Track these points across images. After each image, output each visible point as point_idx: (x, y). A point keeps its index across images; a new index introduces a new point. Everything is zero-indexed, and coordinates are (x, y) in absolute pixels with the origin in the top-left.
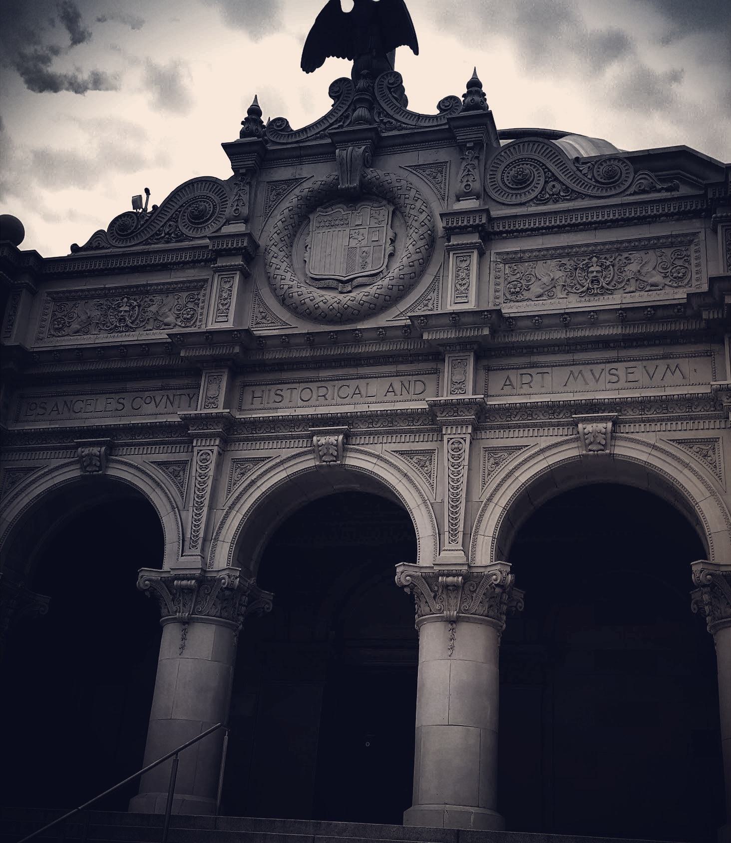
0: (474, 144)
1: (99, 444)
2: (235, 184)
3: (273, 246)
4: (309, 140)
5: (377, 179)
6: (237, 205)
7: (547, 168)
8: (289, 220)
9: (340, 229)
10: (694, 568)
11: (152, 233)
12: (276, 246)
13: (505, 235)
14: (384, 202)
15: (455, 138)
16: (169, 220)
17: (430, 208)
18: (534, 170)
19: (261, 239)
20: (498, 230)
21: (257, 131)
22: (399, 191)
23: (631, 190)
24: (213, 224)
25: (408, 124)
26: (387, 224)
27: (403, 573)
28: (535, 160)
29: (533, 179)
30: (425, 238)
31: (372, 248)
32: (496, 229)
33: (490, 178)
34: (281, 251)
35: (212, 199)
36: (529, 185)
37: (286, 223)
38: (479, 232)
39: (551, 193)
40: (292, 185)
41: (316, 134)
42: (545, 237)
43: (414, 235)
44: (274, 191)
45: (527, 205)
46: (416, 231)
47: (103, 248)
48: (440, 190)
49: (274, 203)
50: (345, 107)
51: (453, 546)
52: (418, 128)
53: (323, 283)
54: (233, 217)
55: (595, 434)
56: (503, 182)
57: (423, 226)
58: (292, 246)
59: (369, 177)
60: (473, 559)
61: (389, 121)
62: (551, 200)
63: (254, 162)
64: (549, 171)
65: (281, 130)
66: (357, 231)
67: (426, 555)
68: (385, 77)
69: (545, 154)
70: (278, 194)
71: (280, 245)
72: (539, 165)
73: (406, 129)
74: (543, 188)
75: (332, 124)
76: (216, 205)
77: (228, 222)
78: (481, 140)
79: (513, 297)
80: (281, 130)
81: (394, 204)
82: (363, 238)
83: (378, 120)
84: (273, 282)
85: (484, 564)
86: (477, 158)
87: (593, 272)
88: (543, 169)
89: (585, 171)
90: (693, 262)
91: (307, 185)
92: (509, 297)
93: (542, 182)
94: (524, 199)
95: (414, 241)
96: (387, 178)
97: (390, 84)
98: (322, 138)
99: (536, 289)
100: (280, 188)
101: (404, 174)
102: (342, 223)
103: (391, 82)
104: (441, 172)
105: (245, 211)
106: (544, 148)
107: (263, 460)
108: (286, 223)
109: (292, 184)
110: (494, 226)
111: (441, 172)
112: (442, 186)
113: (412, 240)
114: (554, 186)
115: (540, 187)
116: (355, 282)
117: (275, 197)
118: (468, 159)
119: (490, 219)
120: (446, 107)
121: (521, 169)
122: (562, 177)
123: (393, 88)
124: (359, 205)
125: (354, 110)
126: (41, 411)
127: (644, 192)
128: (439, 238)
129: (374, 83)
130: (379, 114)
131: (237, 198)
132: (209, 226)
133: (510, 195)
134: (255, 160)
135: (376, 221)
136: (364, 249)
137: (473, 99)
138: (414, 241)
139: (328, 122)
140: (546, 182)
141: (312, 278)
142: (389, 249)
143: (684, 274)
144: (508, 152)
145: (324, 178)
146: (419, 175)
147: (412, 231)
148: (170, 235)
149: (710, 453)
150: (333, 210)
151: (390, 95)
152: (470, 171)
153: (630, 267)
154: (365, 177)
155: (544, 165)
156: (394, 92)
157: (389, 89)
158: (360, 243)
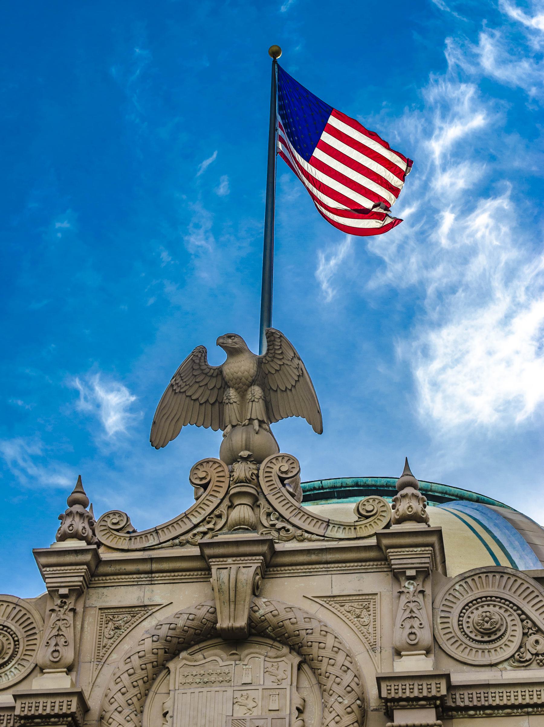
0: (417, 571)
2: (50, 611)
3: (116, 713)
4: (162, 548)
5: (274, 616)
6: (56, 645)
7: (523, 613)
8: (139, 671)
9: (217, 689)
12: (120, 712)
13: (472, 712)
14: (285, 650)
15: (385, 559)
17: (356, 664)
18: (506, 615)
19: (90, 700)
20: (462, 704)
21: (84, 531)
22: (309, 636)
24: (13, 670)
25: (313, 534)
26: (291, 685)
28: (506, 600)
29: (506, 631)
30: (353, 711)
31: (269, 720)
32: (460, 703)
33: (441, 623)
34: (128, 721)
35: (12, 631)
36: (501, 637)
37: (135, 677)
38: (436, 707)
39: (534, 652)
40: (139, 615)
41: (173, 539)
42: (531, 717)
43: (336, 706)
44: (110, 623)
45: (500, 666)
46: (340, 700)
48: (368, 635)
49: (111, 641)
50: (217, 501)
52: (328, 541)
54: (49, 663)
56: (461, 629)
57: (349, 692)
58: (142, 712)
59: (262, 612)
61: (284, 528)
62: (535, 663)
63: (81, 579)
64: (528, 617)
65: (117, 530)
66: (244, 693)
68: (274, 461)
69: (514, 589)
70: (117, 628)
71: (127, 711)
72: (512, 608)
73: (310, 540)
74: (521, 643)
75: (196, 526)
76: (18, 641)
77: (39, 669)
78: (427, 568)
80: (117, 530)
81: (299, 653)
82: (255, 705)
86: (422, 592)
88: (519, 615)
91: (161, 616)
94: (495, 658)
95: (338, 715)
96: (290, 615)
97: (282, 472)
100: (119, 618)
101: (312, 608)
102: (221, 679)
103: (284, 469)
104: (367, 609)
105: (68, 655)
106: (524, 587)
108: (135, 677)
109: (137, 614)
110: (455, 699)
111: (367, 609)
112: (371, 630)
113: (334, 714)
114: (537, 642)
117: (112, 633)
118: (408, 592)
119: (450, 687)
120: (368, 512)
121: (488, 614)
123: (288, 478)
124: (246, 652)
125: (231, 507)
128: (372, 711)
129: (258, 470)
130: (269, 515)
131: (55, 632)
132: (8, 673)
133: (459, 643)
134: (83, 576)
135: (273, 678)
137: (410, 506)
138: (338, 715)
139: (190, 520)
144: (464, 585)
146: (335, 611)
147: (332, 699)
150: (205, 658)
151: (283, 490)
152: (414, 612)
154: (255, 612)
155: (519, 608)
156: (289, 484)
157: (282, 480)
158: (251, 712)
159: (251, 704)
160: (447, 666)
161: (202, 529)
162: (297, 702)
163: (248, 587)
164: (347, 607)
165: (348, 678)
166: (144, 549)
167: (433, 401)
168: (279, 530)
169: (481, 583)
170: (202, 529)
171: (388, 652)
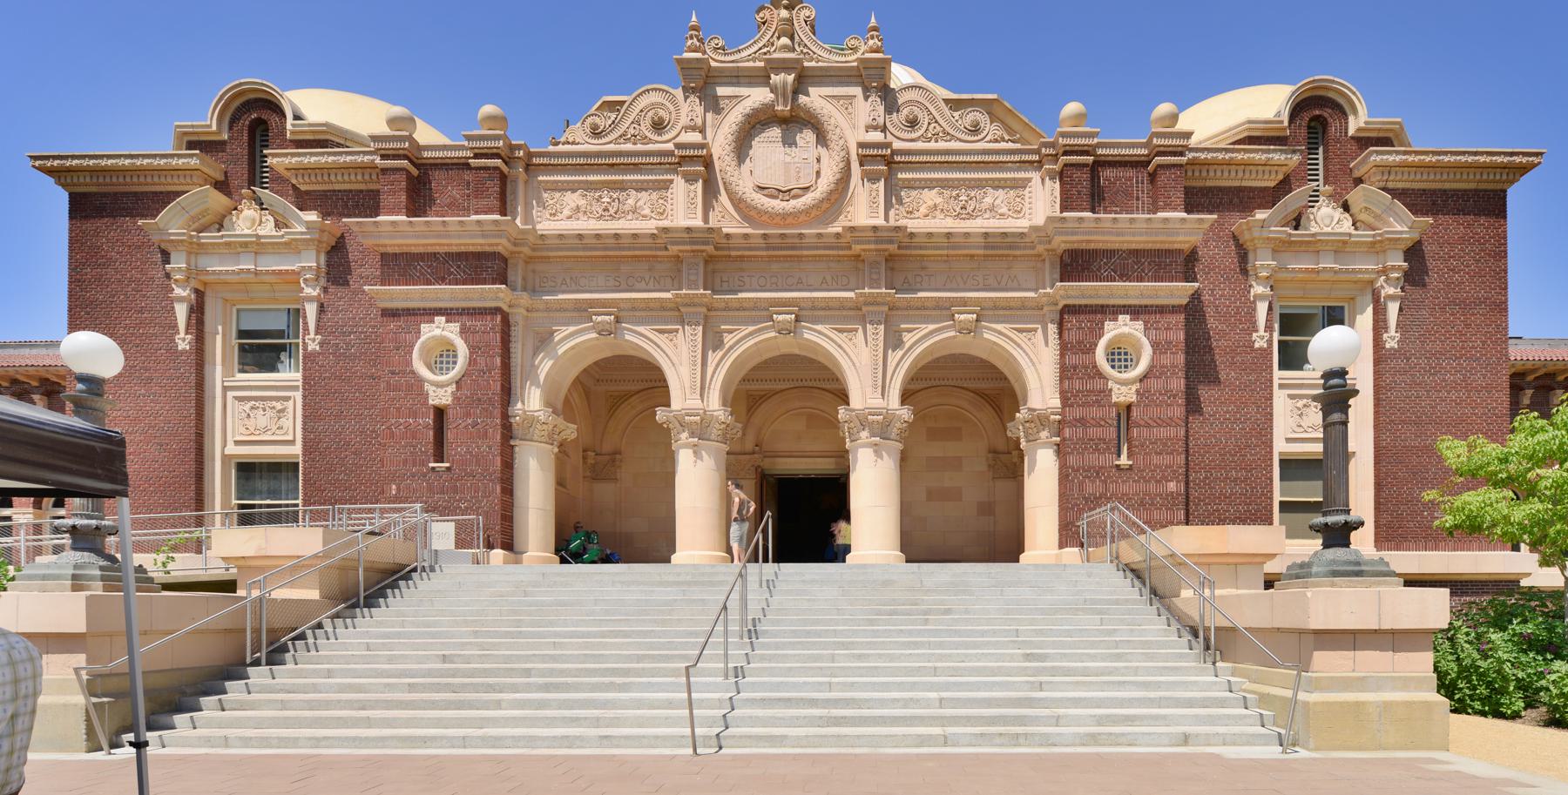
1: (609, 314)
10: (840, 411)
11: (619, 133)
16: (633, 123)
23: (987, 139)
27: (661, 414)
43: (836, 157)
47: (578, 144)
51: (694, 396)
53: (766, 192)
55: (783, 322)
60: (708, 405)
67: (677, 403)
79: (908, 216)
83: (798, 50)
84: (730, 187)
85: (535, 409)
87: (962, 201)
89: (957, 118)
90: (1027, 200)
92: (905, 215)
93: (926, 123)
98: (754, 60)
99: (923, 210)
101: (823, 102)
107: (732, 333)
111: (851, 104)
114: (935, 128)
115: (925, 126)
116: (793, 192)
122: (941, 121)
125: (779, 38)
126: (553, 284)
127: (996, 141)
136: (799, 165)
140: (929, 124)
141: (759, 187)
142: (816, 167)
143: (664, 210)
145: (761, 99)
148: (636, 136)
149: (675, 339)
153: (986, 200)
157: (806, 22)
159: (793, 155)
160: (890, 138)
161: (765, 50)
162: (816, 155)
163: (993, 571)
164: (841, 102)
165: (841, 142)
166: (732, 62)
167: (27, 648)
168: (805, 54)
169: (849, 74)
170: (765, 50)
171: (863, 129)
